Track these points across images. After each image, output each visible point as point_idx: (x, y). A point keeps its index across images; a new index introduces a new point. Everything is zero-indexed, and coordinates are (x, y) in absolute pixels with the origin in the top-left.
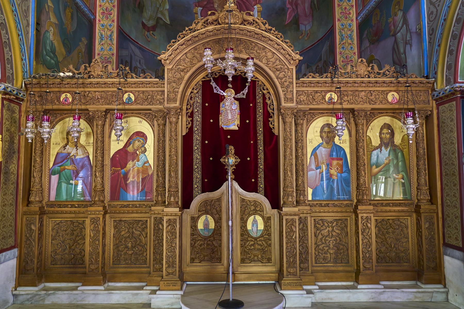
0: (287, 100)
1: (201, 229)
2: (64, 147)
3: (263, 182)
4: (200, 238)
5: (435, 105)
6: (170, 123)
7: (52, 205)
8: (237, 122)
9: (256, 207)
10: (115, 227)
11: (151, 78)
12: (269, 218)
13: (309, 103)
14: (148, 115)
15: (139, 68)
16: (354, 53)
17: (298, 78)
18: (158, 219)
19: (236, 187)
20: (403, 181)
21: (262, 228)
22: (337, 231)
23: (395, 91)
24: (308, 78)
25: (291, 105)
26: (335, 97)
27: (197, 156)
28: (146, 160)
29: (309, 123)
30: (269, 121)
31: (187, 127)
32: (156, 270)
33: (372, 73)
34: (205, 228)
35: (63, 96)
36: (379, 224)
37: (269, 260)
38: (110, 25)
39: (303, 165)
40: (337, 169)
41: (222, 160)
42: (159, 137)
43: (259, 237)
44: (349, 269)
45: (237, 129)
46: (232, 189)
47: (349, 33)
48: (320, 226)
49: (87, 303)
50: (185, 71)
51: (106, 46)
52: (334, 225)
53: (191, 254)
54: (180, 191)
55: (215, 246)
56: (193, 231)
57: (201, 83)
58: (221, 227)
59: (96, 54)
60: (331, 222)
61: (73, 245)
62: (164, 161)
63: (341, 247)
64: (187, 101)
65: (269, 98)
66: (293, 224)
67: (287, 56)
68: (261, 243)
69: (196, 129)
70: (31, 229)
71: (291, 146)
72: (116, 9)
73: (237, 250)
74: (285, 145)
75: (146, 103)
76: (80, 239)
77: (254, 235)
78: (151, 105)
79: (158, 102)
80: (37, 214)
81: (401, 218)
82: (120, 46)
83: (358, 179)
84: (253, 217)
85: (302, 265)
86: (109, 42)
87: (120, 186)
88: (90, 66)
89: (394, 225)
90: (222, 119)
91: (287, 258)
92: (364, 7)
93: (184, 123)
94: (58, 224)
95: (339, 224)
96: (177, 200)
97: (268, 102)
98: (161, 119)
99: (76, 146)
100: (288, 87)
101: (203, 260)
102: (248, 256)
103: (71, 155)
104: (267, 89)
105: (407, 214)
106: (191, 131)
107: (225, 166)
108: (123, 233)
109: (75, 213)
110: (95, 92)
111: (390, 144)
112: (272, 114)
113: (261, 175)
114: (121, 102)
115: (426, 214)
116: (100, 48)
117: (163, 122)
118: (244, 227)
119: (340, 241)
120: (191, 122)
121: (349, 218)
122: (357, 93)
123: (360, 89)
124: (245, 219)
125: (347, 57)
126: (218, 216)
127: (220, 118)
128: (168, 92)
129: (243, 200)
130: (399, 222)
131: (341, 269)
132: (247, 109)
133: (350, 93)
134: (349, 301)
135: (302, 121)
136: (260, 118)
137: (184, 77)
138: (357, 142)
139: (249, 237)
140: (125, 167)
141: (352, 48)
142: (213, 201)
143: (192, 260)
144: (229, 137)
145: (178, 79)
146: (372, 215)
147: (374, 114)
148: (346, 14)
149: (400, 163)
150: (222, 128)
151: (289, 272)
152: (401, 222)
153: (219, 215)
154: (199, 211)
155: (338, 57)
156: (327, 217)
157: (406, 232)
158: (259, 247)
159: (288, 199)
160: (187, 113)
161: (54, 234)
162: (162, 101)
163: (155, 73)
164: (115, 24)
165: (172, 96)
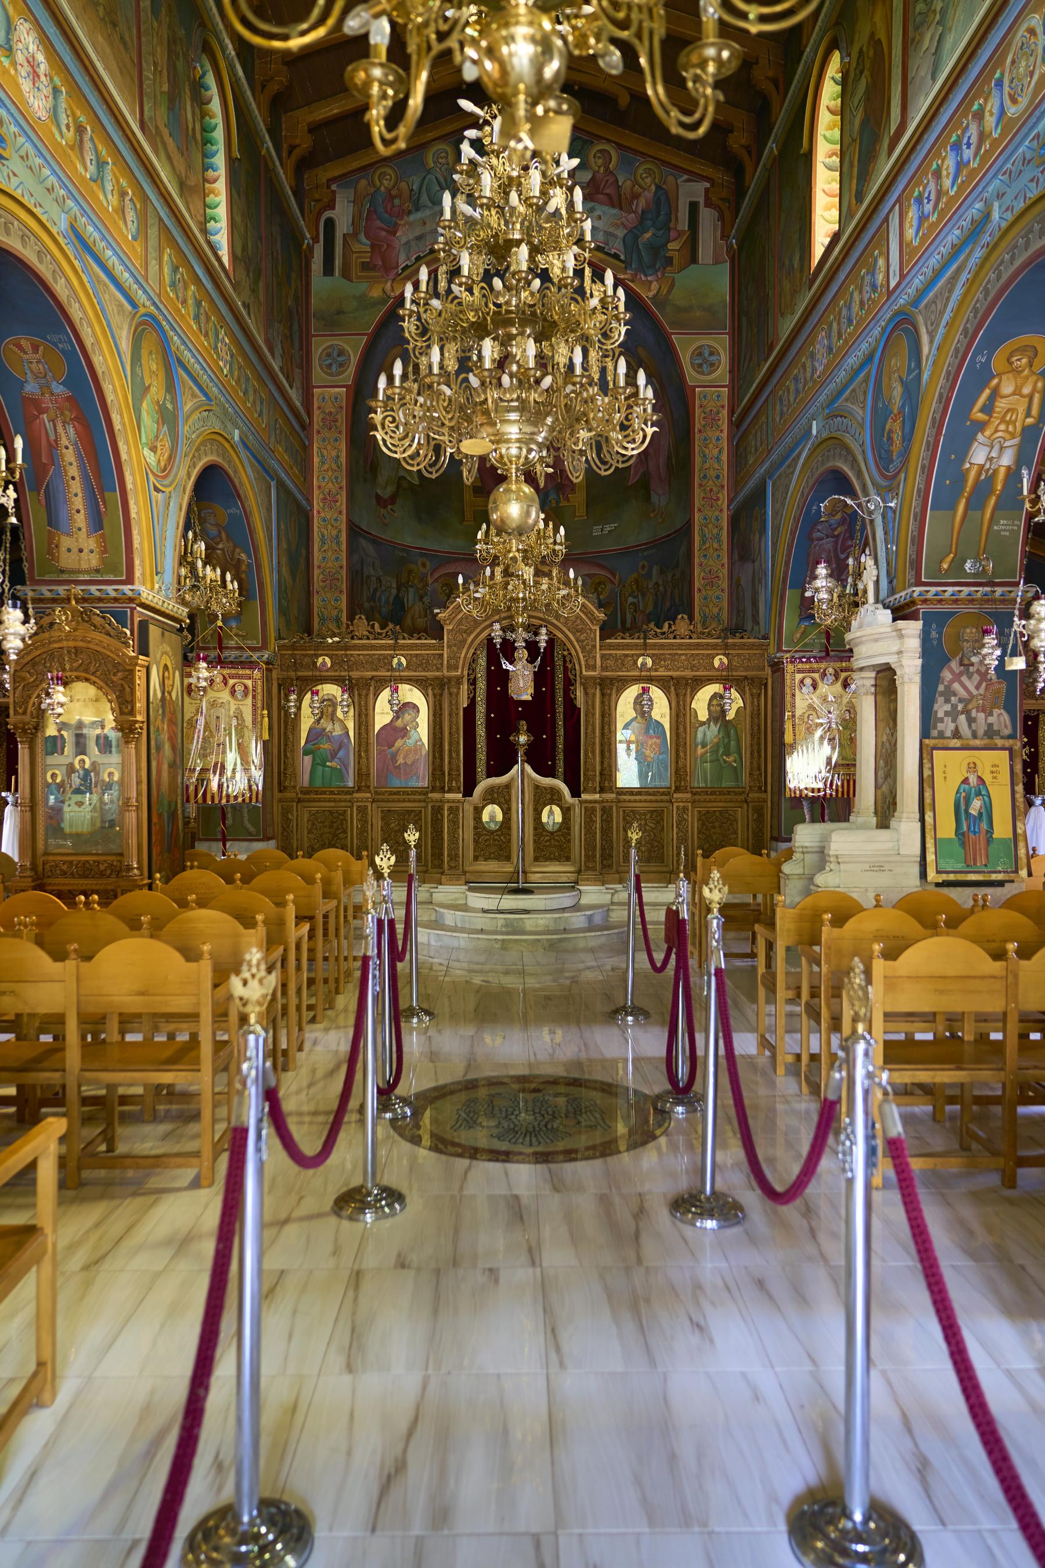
2: (318, 721)
7: (306, 792)
8: (531, 691)
9: (552, 795)
10: (383, 819)
14: (420, 683)
26: (649, 662)
27: (481, 732)
32: (434, 866)
37: (568, 859)
38: (336, 520)
44: (664, 869)
47: (715, 531)
51: (330, 553)
82: (351, 550)
86: (335, 547)
90: (512, 687)
92: (736, 494)
97: (570, 666)
100: (590, 651)
106: (473, 702)
113: (560, 756)
129: (537, 787)
132: (542, 679)
136: (559, 686)
138: (677, 716)
143: (476, 858)
147: (699, 683)
148: (711, 500)
164: (344, 517)
165: (452, 662)
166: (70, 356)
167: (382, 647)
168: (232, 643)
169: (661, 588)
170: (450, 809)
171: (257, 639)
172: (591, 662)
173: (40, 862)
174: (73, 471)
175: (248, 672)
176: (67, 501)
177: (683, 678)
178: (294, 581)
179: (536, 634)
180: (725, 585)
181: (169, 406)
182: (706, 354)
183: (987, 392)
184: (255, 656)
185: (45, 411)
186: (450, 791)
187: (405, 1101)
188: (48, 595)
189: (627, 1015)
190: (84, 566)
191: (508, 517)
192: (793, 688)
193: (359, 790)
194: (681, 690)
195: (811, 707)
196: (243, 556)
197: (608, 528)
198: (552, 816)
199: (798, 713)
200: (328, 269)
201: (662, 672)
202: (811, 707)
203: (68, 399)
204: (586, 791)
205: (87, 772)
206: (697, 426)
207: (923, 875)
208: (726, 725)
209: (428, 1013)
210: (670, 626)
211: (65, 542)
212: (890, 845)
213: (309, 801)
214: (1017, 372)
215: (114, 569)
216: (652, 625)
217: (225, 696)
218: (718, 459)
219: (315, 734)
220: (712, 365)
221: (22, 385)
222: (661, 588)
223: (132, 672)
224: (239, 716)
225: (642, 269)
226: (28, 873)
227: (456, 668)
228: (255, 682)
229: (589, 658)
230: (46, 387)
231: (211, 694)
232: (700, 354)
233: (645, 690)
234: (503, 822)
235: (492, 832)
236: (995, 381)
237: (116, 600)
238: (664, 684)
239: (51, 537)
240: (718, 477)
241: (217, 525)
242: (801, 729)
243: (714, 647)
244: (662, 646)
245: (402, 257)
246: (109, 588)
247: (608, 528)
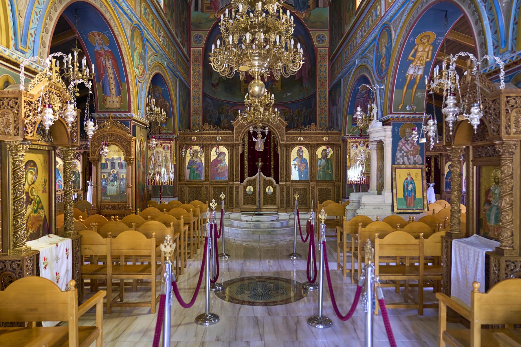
0: (282, 140)
2: (192, 158)
8: (263, 148)
12: (275, 187)
17: (286, 131)
26: (302, 139)
27: (246, 162)
29: (292, 149)
37: (275, 204)
46: (259, 175)
62: (233, 164)
72: (201, 83)
74: (281, 158)
82: (203, 101)
83: (286, 172)
100: (282, 135)
113: (272, 170)
129: (265, 180)
136: (272, 146)
143: (244, 204)
147: (318, 146)
148: (323, 85)
155: (318, 108)
164: (201, 90)
166: (110, 38)
167: (213, 134)
170: (236, 187)
171: (172, 131)
172: (283, 139)
173: (99, 205)
174: (111, 75)
176: (109, 85)
178: (184, 111)
179: (264, 129)
180: (327, 113)
181: (143, 54)
182: (321, 37)
183: (414, 50)
184: (171, 136)
185: (102, 56)
187: (220, 285)
188: (103, 116)
189: (294, 256)
190: (115, 107)
191: (255, 91)
192: (350, 147)
193: (206, 181)
194: (312, 148)
197: (288, 94)
198: (270, 190)
199: (351, 156)
200: (196, 9)
202: (356, 154)
203: (110, 52)
204: (281, 181)
205: (115, 175)
206: (318, 61)
207: (393, 210)
208: (327, 160)
209: (228, 255)
211: (109, 99)
212: (382, 200)
214: (424, 44)
215: (125, 108)
216: (303, 127)
217: (161, 149)
218: (325, 72)
219: (191, 162)
220: (323, 41)
221: (94, 47)
223: (130, 142)
224: (166, 156)
225: (300, 9)
226: (95, 208)
227: (238, 141)
230: (102, 48)
231: (157, 149)
232: (319, 37)
233: (301, 148)
235: (250, 195)
236: (416, 47)
237: (125, 118)
238: (307, 146)
239: (104, 97)
240: (325, 78)
241: (159, 93)
242: (353, 161)
243: (324, 134)
244: (306, 134)
245: (221, 5)
246: (123, 114)
247: (288, 94)
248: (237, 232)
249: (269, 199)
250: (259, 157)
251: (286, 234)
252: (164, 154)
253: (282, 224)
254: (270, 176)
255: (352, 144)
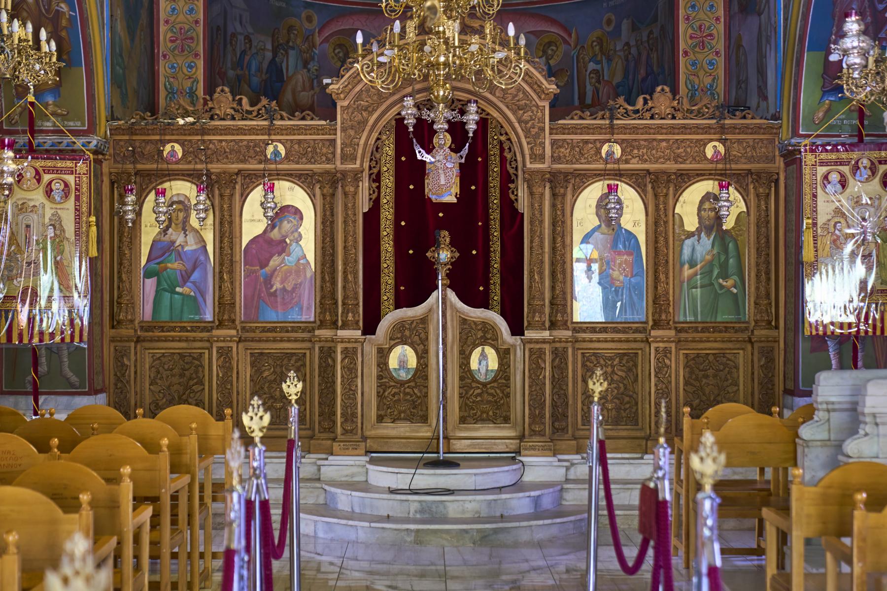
0: (535, 158)
1: (395, 369)
2: (165, 231)
3: (499, 292)
4: (393, 384)
5: (782, 165)
6: (345, 194)
7: (148, 327)
8: (456, 189)
9: (485, 332)
10: (253, 365)
11: (312, 119)
12: (507, 352)
13: (574, 160)
14: (305, 180)
15: (241, 34)
16: (718, 19)
18: (325, 349)
19: (453, 299)
20: (735, 291)
21: (496, 368)
22: (620, 373)
23: (719, 140)
24: (572, 119)
25: (541, 166)
26: (617, 150)
27: (387, 246)
28: (300, 254)
29: (577, 191)
30: (510, 188)
31: (370, 199)
32: (324, 430)
33: (679, 110)
34: (400, 366)
35: (168, 148)
36: (691, 363)
37: (506, 420)
39: (564, 263)
40: (624, 270)
41: (429, 254)
42: (325, 215)
43: (490, 383)
44: (638, 434)
45: (455, 200)
46: (443, 302)
48: (592, 365)
49: (218, 477)
50: (370, 109)
52: (615, 363)
53: (378, 409)
54: (361, 304)
55: (417, 397)
56: (381, 371)
57: (394, 123)
58: (427, 366)
59: (162, 22)
60: (611, 359)
61: (184, 394)
63: (627, 399)
64: (369, 155)
65: (510, 149)
66: (540, 357)
67: (535, 86)
68: (493, 391)
69: (385, 201)
70: (123, 365)
71: (541, 232)
73: (453, 402)
74: (532, 231)
75: (304, 159)
76: (196, 384)
77: (482, 378)
78: (312, 163)
79: (324, 158)
80: (132, 341)
81: (728, 351)
84: (480, 349)
85: (556, 424)
87: (259, 297)
88: (211, 100)
89: (717, 364)
91: (530, 409)
93: (366, 193)
94: (159, 359)
95: (624, 362)
96: (357, 318)
97: (508, 156)
98: (327, 186)
99: (184, 230)
100: (537, 136)
101: (398, 419)
102: (472, 412)
103: (177, 244)
104: (506, 134)
105: (738, 346)
106: (376, 205)
107: (434, 264)
108: (266, 374)
109: (187, 340)
110: (221, 141)
111: (715, 228)
112: (513, 177)
113: (496, 279)
114: (263, 158)
115: (763, 344)
116: (169, 9)
117: (331, 191)
118: (466, 366)
119: (625, 388)
120: (376, 190)
121: (640, 352)
122: (655, 143)
123: (660, 137)
124: (467, 353)
125: (700, 26)
126: (422, 347)
127: (426, 181)
128: (342, 144)
129: (464, 321)
130: (725, 359)
131: (624, 434)
132: (471, 173)
133: (642, 143)
134: (629, 478)
135: (562, 191)
136: (494, 183)
137: (367, 121)
139: (473, 381)
140: (267, 265)
141: (712, 6)
142: (415, 323)
143: (380, 419)
144: (441, 215)
145: (359, 123)
146: (673, 345)
147: (684, 179)
149: (731, 261)
150: (429, 199)
151: (533, 431)
152: (729, 359)
153: (425, 346)
154: (391, 339)
155: (682, 27)
156: (603, 349)
157: (735, 375)
158: (490, 398)
159: (534, 317)
160: (370, 175)
161: (152, 376)
162: (330, 156)
163: (270, 39)
165: (348, 150)
167: (252, 131)
168: (48, 125)
169: (634, 51)
170: (345, 351)
172: (538, 150)
175: (69, 164)
177: (664, 172)
178: (132, 40)
179: (463, 112)
180: (721, 46)
184: (79, 143)
186: (345, 326)
194: (660, 188)
195: (838, 212)
196: (64, 7)
198: (485, 361)
199: (821, 221)
201: (635, 165)
202: (838, 212)
204: (531, 326)
208: (723, 238)
210: (646, 102)
213: (151, 340)
216: (621, 100)
217: (37, 197)
219: (162, 250)
222: (634, 51)
224: (56, 223)
227: (354, 159)
228: (78, 178)
229: (534, 144)
234: (417, 370)
235: (402, 383)
238: (638, 180)
242: (826, 242)
243: (706, 130)
244: (635, 129)
248: (352, 536)
249: (484, 401)
250: (442, 225)
251: (552, 541)
252: (48, 213)
253: (537, 500)
254: (486, 305)
255: (821, 170)
